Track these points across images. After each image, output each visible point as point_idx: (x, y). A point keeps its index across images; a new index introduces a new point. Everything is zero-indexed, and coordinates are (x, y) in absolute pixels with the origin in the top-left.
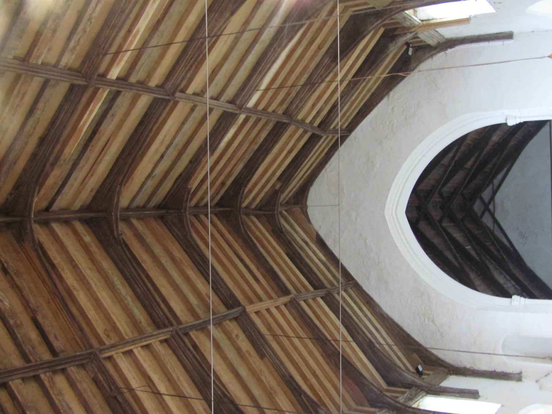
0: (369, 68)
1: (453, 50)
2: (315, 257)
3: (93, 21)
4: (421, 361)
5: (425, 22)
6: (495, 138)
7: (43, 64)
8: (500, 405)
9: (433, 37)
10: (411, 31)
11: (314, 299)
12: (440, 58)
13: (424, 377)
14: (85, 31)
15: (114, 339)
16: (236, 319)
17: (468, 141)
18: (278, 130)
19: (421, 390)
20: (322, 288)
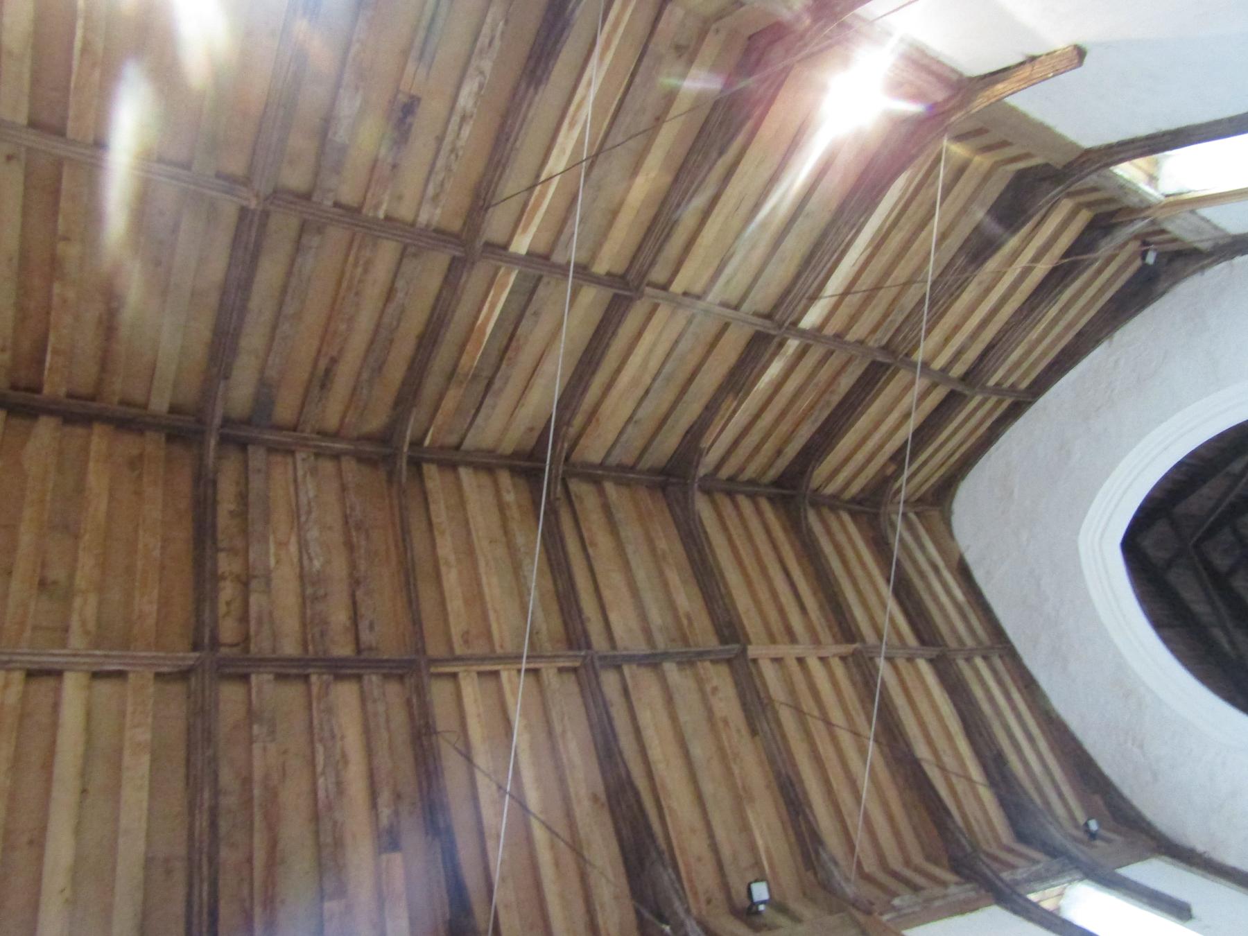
0: (1062, 281)
2: (943, 597)
3: (461, 153)
5: (1171, 199)
7: (388, 218)
11: (910, 660)
12: (1218, 272)
13: (1098, 843)
14: (448, 169)
15: (479, 649)
16: (729, 662)
18: (872, 379)
19: (1077, 868)
20: (933, 645)
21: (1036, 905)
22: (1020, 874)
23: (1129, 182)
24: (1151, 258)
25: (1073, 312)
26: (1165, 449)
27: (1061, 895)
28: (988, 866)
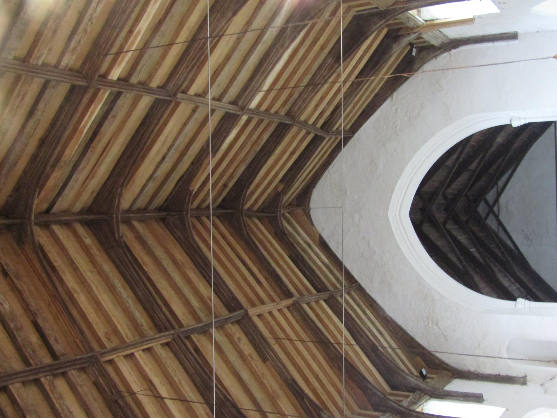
0: (373, 69)
1: (457, 50)
3: (94, 21)
4: (424, 365)
5: (428, 23)
6: (500, 139)
7: (43, 64)
8: (504, 409)
9: (437, 38)
10: (415, 31)
11: (317, 302)
12: (444, 59)
13: (428, 380)
14: (85, 31)
15: (115, 343)
16: (238, 322)
17: (472, 143)
18: (280, 131)
19: (425, 394)
20: (325, 291)
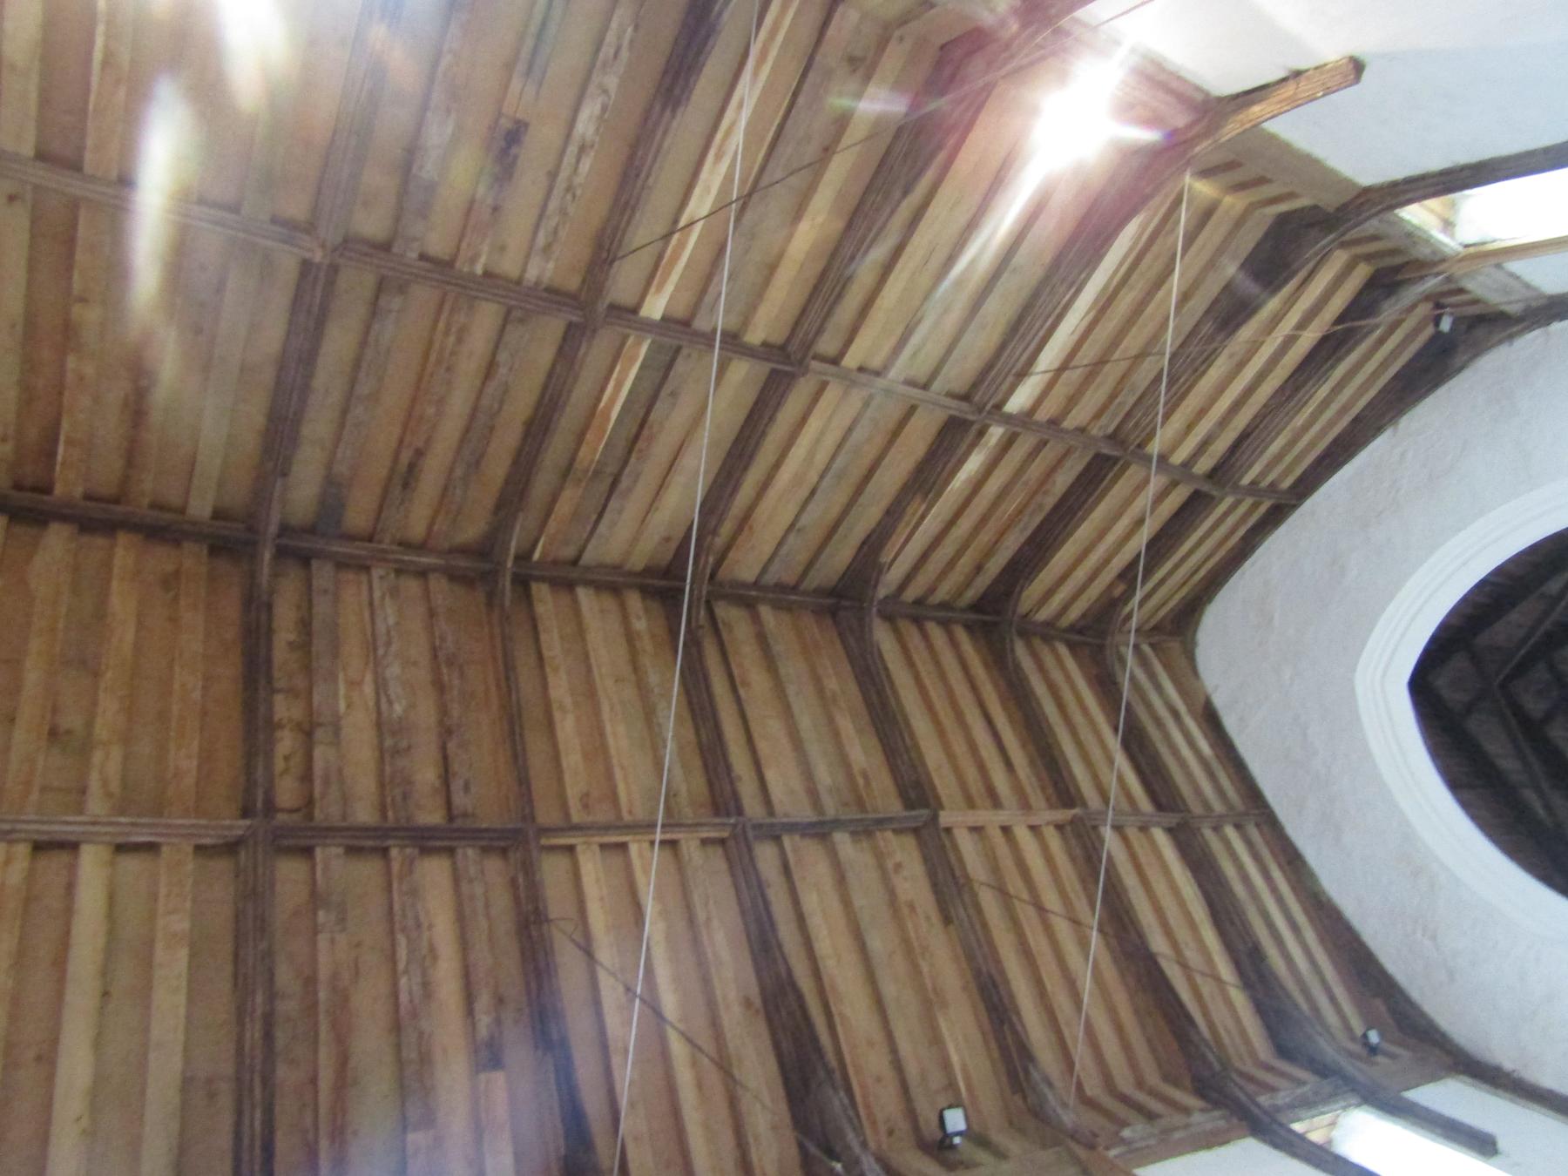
0: (1334, 352)
3: (579, 192)
5: (1472, 250)
7: (487, 274)
11: (1144, 829)
12: (1530, 342)
13: (1380, 1059)
14: (563, 212)
15: (602, 815)
16: (916, 831)
18: (1096, 476)
19: (1353, 1090)
20: (1173, 810)
21: (1301, 1137)
22: (1282, 1098)
23: (1418, 228)
24: (1446, 325)
25: (1348, 392)
26: (1464, 564)
27: (1333, 1124)
28: (1241, 1088)
